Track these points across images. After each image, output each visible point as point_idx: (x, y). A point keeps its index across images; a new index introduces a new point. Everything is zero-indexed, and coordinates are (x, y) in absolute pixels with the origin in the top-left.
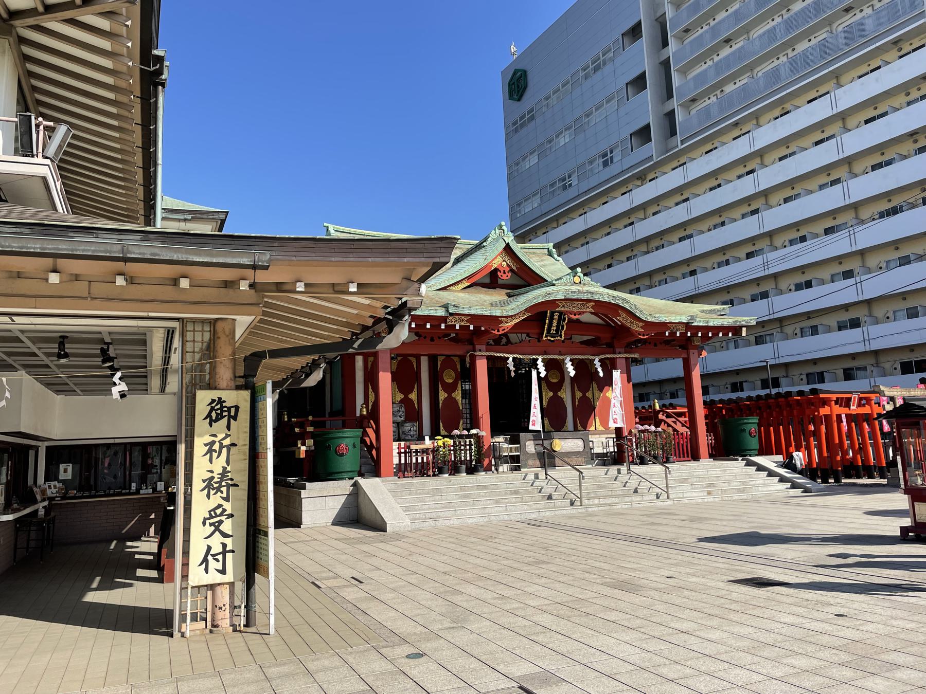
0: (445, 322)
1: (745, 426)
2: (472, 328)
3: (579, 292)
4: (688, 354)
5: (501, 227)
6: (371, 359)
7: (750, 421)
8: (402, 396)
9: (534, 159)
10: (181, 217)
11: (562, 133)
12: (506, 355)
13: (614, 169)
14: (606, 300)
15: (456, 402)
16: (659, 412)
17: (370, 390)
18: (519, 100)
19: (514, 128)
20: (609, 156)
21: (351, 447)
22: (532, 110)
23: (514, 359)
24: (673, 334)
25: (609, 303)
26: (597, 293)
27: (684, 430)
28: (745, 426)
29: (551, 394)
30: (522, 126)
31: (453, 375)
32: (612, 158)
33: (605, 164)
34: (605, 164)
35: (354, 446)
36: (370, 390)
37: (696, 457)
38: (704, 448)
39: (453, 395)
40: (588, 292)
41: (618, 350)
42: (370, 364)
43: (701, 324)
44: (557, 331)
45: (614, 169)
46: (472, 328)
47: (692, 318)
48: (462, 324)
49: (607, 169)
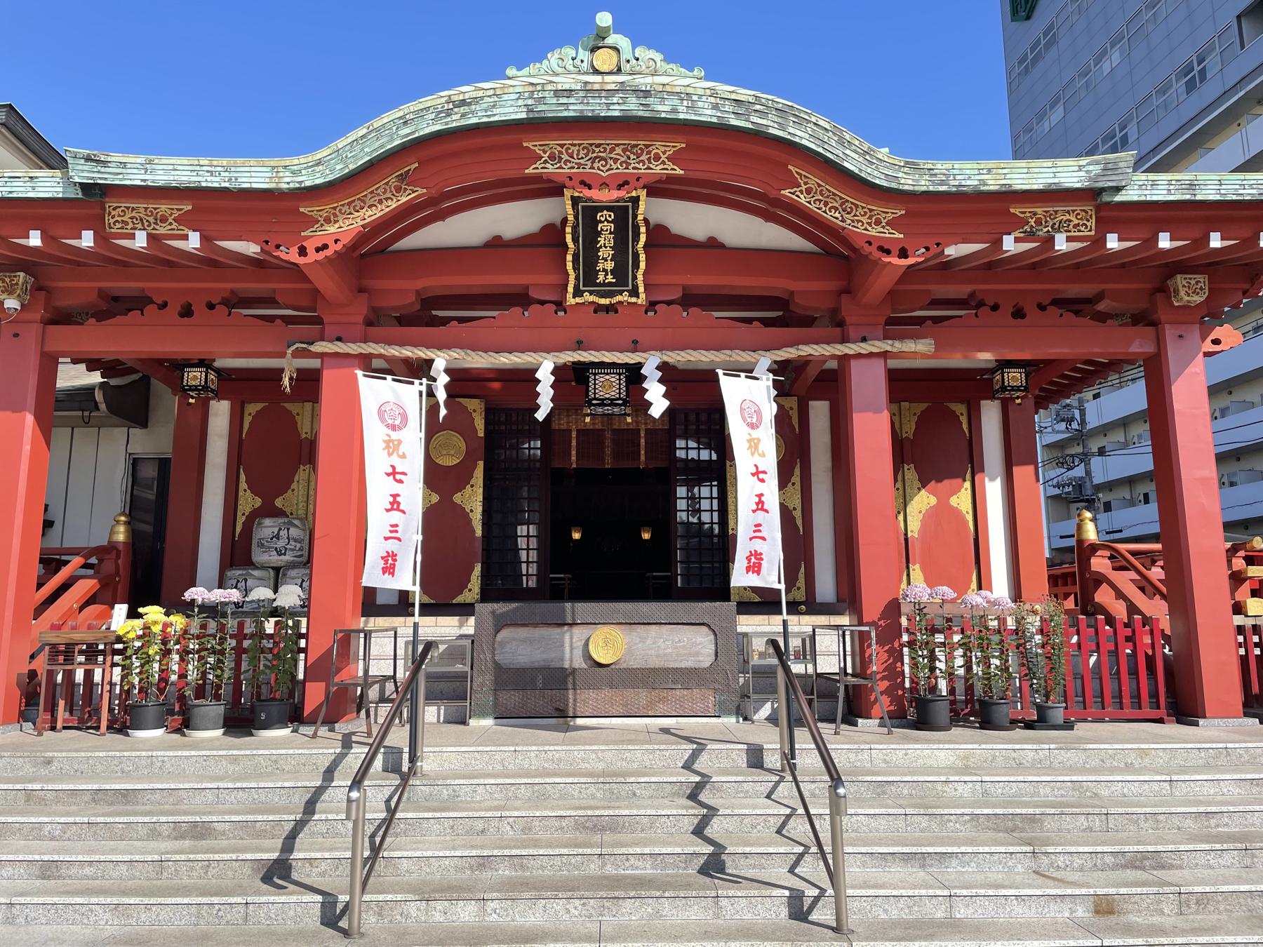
4: (1160, 341)
9: (1057, 114)
11: (1105, 52)
13: (1209, 91)
14: (707, 114)
15: (465, 517)
16: (1094, 548)
17: (799, 522)
18: (1028, 18)
19: (1023, 67)
20: (1197, 69)
22: (1051, 27)
27: (1157, 609)
30: (1035, 61)
31: (463, 445)
32: (1203, 73)
33: (1191, 86)
34: (1191, 86)
36: (799, 522)
37: (1183, 705)
39: (457, 498)
41: (852, 333)
42: (247, 420)
44: (621, 273)
45: (1209, 91)
48: (162, 230)
49: (1195, 94)
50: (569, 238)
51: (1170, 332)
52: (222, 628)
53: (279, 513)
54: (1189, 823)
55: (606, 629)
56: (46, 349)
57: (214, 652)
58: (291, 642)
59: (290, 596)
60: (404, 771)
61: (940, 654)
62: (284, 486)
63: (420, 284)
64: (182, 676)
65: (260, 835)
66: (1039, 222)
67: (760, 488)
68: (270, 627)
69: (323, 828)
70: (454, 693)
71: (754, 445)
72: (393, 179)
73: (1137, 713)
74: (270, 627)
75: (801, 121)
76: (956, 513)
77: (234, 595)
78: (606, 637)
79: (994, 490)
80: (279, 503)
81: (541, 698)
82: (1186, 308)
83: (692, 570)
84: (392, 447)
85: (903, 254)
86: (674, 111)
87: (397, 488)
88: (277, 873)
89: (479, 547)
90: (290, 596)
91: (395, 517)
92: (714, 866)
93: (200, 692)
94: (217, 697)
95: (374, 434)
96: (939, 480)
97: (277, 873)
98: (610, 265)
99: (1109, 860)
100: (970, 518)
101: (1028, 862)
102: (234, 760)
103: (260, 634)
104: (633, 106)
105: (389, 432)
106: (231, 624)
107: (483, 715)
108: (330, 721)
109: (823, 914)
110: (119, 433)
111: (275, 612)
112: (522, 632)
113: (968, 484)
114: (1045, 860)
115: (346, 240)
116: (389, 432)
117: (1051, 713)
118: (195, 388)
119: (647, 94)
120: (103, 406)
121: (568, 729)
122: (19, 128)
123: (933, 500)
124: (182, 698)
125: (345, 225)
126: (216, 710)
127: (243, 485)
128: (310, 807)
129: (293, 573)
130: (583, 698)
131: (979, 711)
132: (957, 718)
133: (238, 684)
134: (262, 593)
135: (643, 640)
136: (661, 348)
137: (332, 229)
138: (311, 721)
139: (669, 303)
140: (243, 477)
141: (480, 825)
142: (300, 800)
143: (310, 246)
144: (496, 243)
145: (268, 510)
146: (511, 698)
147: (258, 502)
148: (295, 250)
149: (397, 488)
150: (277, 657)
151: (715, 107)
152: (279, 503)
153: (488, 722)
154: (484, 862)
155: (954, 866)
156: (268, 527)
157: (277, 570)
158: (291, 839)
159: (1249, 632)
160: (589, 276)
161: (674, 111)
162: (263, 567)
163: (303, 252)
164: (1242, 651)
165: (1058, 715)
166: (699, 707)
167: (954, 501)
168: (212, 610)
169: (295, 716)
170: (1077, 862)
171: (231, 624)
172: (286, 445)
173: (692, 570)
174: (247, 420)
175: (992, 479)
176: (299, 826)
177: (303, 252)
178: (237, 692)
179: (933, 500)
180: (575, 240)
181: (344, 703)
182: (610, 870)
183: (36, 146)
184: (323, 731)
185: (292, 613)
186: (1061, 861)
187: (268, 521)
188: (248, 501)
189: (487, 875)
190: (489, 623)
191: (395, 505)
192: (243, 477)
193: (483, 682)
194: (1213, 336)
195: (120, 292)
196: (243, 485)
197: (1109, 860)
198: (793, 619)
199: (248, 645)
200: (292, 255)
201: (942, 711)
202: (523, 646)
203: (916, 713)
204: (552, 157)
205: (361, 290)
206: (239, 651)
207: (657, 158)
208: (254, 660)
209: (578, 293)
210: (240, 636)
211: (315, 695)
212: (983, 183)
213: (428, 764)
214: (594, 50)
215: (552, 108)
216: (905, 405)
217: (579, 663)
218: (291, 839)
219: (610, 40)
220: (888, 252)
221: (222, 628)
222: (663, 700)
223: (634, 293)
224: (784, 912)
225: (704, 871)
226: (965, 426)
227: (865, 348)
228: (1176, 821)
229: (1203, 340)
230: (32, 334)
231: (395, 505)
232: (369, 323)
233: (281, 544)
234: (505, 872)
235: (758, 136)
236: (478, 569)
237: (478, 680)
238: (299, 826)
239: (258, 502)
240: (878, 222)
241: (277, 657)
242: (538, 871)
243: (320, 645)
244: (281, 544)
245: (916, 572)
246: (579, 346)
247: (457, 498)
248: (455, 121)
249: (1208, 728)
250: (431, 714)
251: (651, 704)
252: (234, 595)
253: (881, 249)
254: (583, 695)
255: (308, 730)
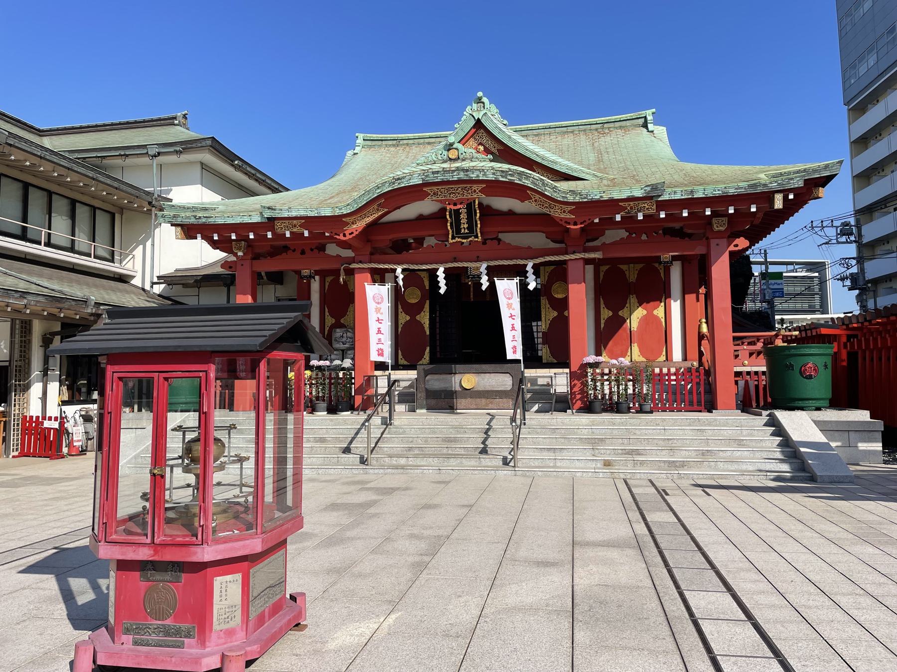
0: (272, 230)
1: (793, 361)
2: (306, 234)
3: (445, 171)
5: (479, 101)
6: (329, 279)
7: (808, 351)
8: (611, 313)
10: (171, 149)
12: (522, 262)
14: (491, 177)
21: (821, 368)
23: (404, 270)
24: (629, 220)
25: (497, 182)
26: (473, 170)
28: (793, 361)
29: (555, 314)
31: (419, 293)
35: (826, 366)
37: (711, 406)
38: (726, 389)
39: (418, 318)
40: (458, 169)
42: (327, 284)
43: (678, 196)
44: (471, 228)
46: (306, 234)
47: (654, 187)
48: (295, 230)
50: (448, 217)
51: (713, 242)
52: (323, 375)
53: (342, 326)
54: (661, 442)
55: (468, 375)
56: (254, 269)
57: (321, 384)
58: (349, 380)
59: (347, 363)
60: (387, 422)
61: (598, 384)
62: (344, 313)
63: (391, 237)
64: (311, 393)
65: (341, 441)
66: (631, 208)
67: (513, 322)
68: (341, 375)
69: (360, 439)
70: (408, 398)
71: (509, 306)
72: (376, 206)
73: (691, 408)
74: (341, 375)
75: (527, 177)
76: (657, 318)
77: (327, 363)
78: (468, 379)
79: (676, 307)
80: (342, 321)
81: (444, 401)
82: (719, 231)
83: (491, 353)
84: (378, 310)
85: (575, 224)
86: (478, 176)
87: (380, 326)
88: (347, 450)
89: (428, 339)
90: (347, 363)
91: (380, 336)
92: (484, 451)
93: (317, 398)
94: (324, 400)
95: (371, 306)
96: (648, 302)
97: (347, 450)
98: (466, 226)
99: (620, 451)
100: (663, 320)
101: (591, 451)
102: (331, 420)
103: (338, 377)
104: (462, 175)
105: (377, 302)
106: (327, 373)
107: (422, 408)
108: (364, 409)
109: (512, 464)
110: (271, 287)
111: (343, 369)
112: (436, 377)
113: (663, 304)
114: (597, 451)
115: (360, 230)
116: (377, 302)
117: (644, 407)
118: (306, 277)
119: (467, 171)
120: (265, 278)
121: (453, 413)
122: (217, 147)
123: (645, 312)
124: (311, 401)
125: (359, 225)
126: (324, 405)
127: (327, 313)
128: (357, 434)
129: (349, 352)
130: (460, 402)
131: (614, 407)
132: (605, 410)
133: (330, 397)
134: (337, 362)
135: (483, 379)
136: (487, 260)
137: (355, 226)
138: (357, 410)
139: (492, 239)
140: (327, 310)
141: (411, 439)
142: (353, 432)
143: (347, 233)
144: (421, 218)
145: (338, 325)
146: (433, 402)
147: (334, 321)
148: (342, 235)
149: (380, 326)
150: (344, 386)
151: (494, 174)
152: (342, 321)
153: (424, 411)
154: (410, 449)
155: (565, 453)
156: (338, 333)
157: (343, 351)
158: (351, 442)
159: (752, 374)
160: (458, 230)
161: (478, 176)
162: (337, 350)
163: (344, 235)
164: (756, 383)
165: (647, 408)
166: (506, 406)
167: (655, 312)
168: (319, 368)
169: (352, 408)
170: (608, 452)
171: (327, 373)
172: (342, 303)
173: (491, 353)
174: (327, 284)
175: (675, 301)
176: (353, 439)
177: (344, 235)
178: (330, 397)
179: (645, 312)
180: (451, 217)
181: (369, 404)
182: (450, 452)
183: (225, 153)
184: (362, 413)
185: (349, 369)
186: (602, 451)
187: (338, 330)
188: (330, 321)
189: (412, 453)
190: (422, 374)
191: (379, 332)
192: (327, 310)
193: (421, 395)
194: (734, 243)
195: (280, 248)
196: (327, 313)
197: (620, 451)
198: (392, 372)
199: (334, 382)
200: (341, 237)
201: (597, 405)
202: (436, 382)
203: (588, 408)
204: (434, 194)
205: (368, 241)
206: (330, 384)
207: (475, 191)
208: (336, 387)
209: (453, 238)
210: (330, 378)
211: (358, 400)
212: (601, 197)
213: (396, 421)
214: (448, 150)
215: (431, 178)
216: (632, 265)
217: (458, 388)
218: (351, 442)
219: (454, 146)
220: (569, 224)
221: (323, 375)
222: (491, 403)
223: (477, 237)
224: (501, 463)
225: (481, 453)
226: (662, 275)
227: (573, 257)
228: (656, 441)
229: (729, 245)
230: (247, 263)
231: (379, 332)
232: (372, 254)
233: (344, 340)
234: (416, 452)
235: (511, 183)
236: (428, 349)
237: (419, 395)
238: (353, 439)
239: (334, 321)
240: (564, 212)
241: (344, 386)
242: (427, 451)
243: (359, 381)
244: (344, 340)
245: (635, 348)
246: (455, 260)
247: (418, 318)
248: (396, 186)
249: (716, 415)
250: (400, 408)
251: (487, 404)
252: (327, 363)
253: (566, 222)
254: (459, 401)
255: (356, 413)
